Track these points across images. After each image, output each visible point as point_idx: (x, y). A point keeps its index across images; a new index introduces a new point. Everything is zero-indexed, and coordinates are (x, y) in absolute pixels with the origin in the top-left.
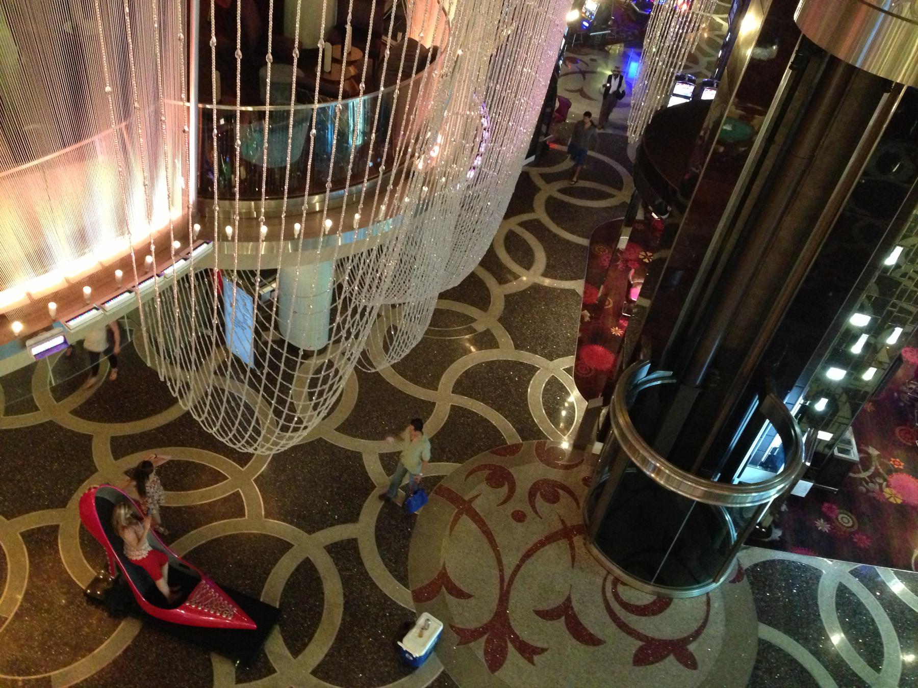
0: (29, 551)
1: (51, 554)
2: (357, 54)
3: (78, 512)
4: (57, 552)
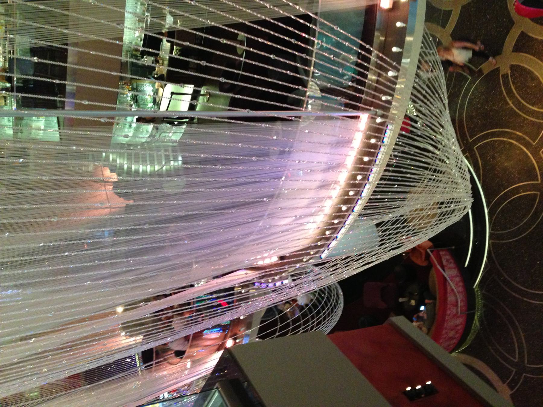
0: (526, 52)
1: (535, 44)
2: (192, 304)
3: (522, 18)
4: (536, 39)
